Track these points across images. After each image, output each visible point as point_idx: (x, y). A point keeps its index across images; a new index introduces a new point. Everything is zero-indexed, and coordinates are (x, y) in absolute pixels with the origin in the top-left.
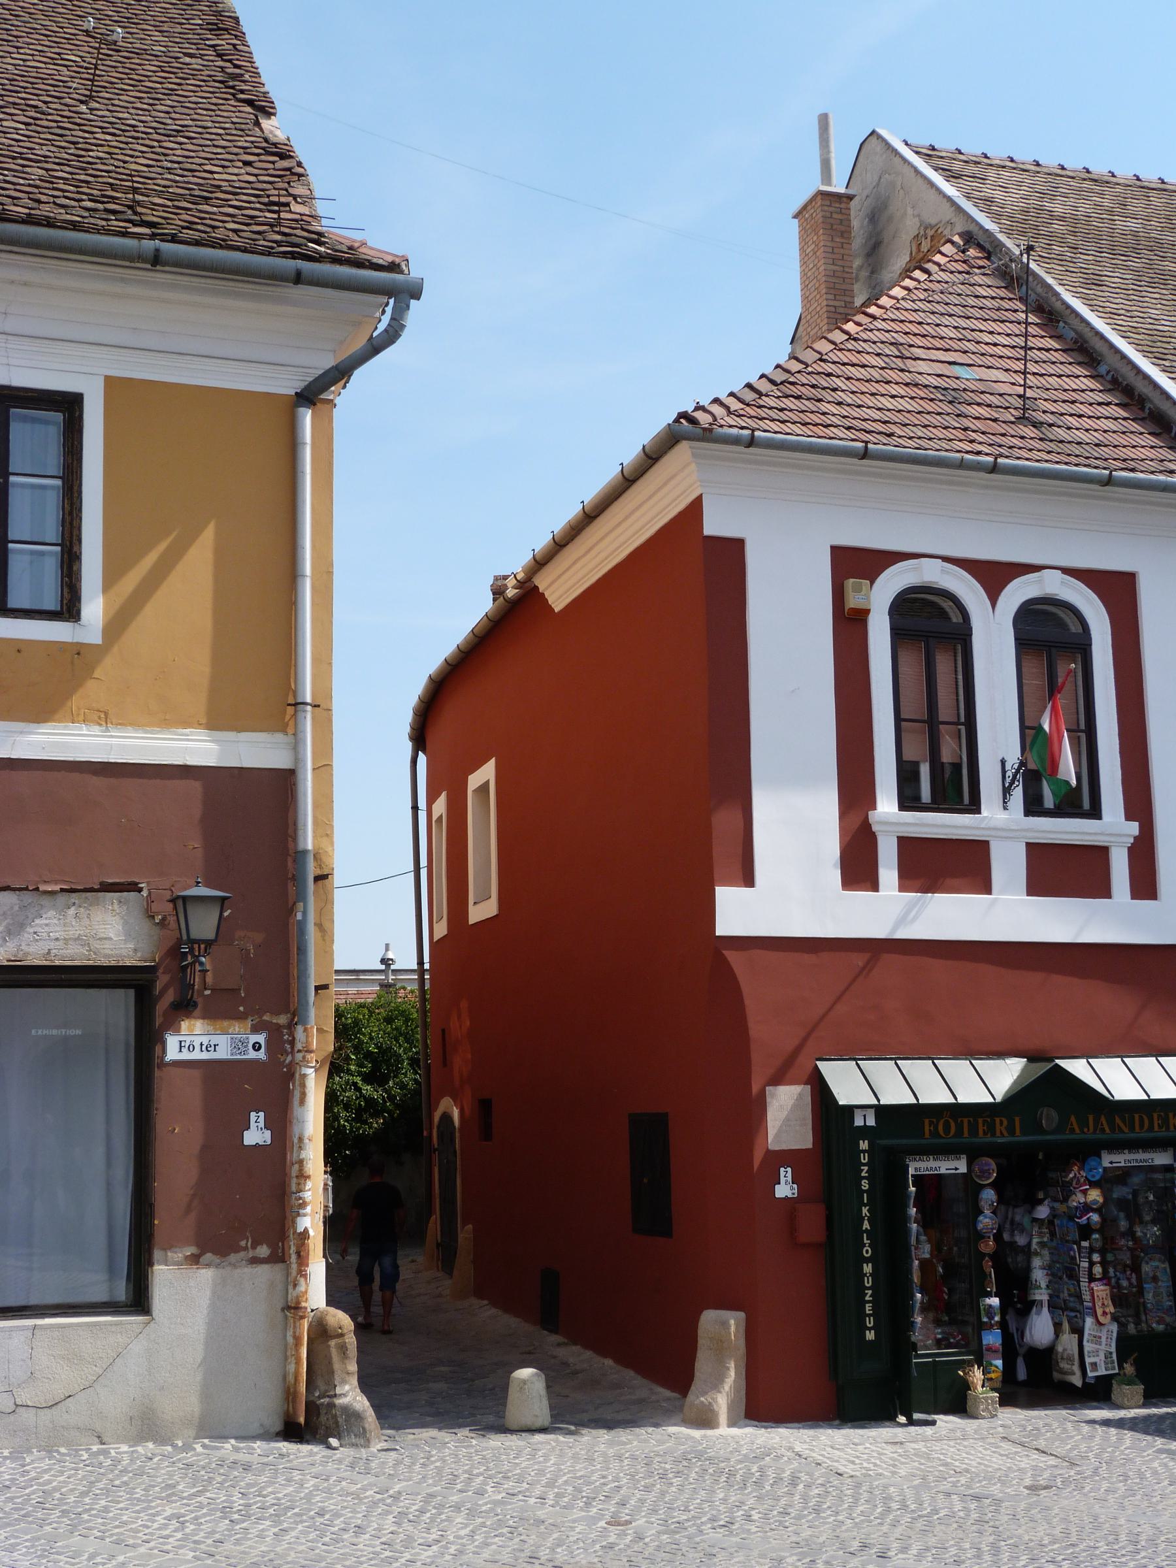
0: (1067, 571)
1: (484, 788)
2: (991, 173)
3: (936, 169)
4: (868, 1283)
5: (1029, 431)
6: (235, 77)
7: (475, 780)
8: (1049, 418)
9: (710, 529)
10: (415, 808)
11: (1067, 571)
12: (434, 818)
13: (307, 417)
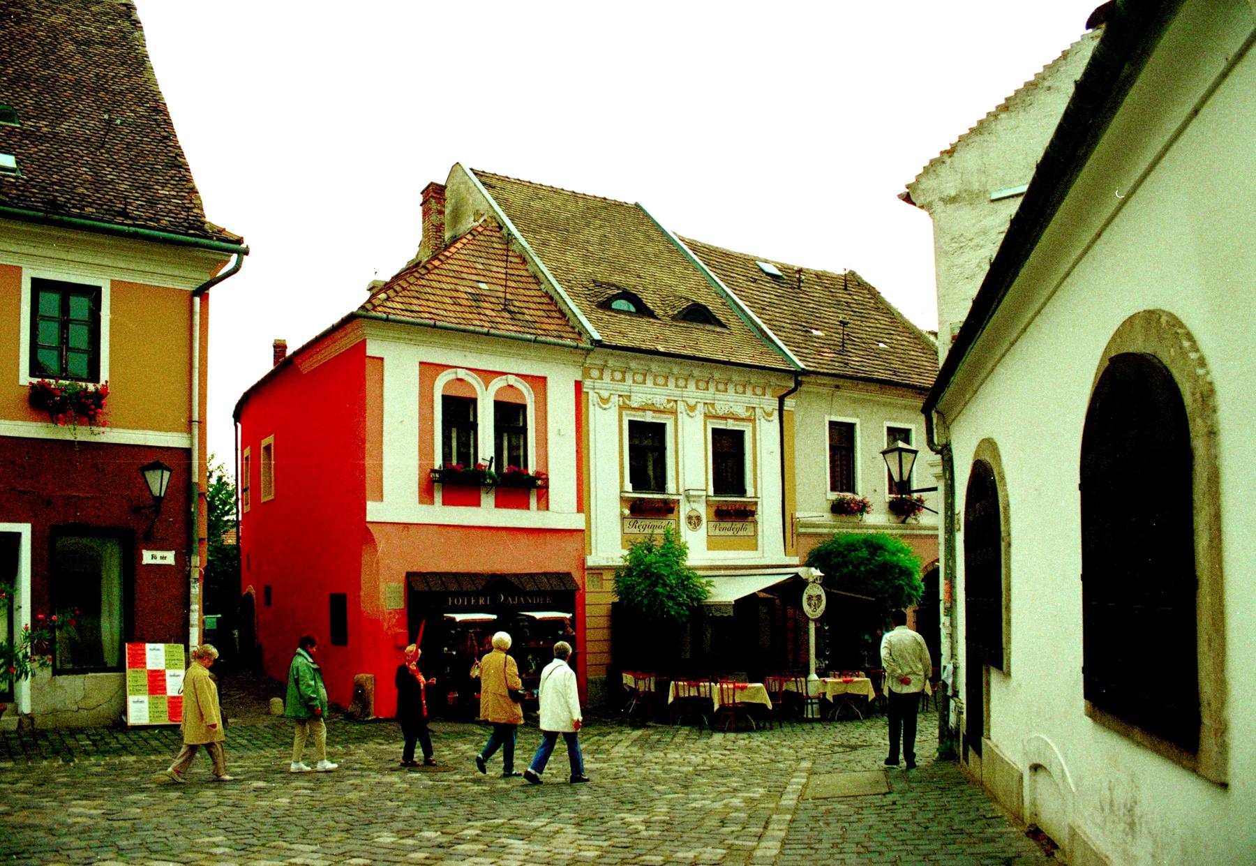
0: (517, 375)
1: (268, 448)
2: (509, 186)
3: (484, 184)
4: (902, 738)
5: (506, 315)
6: (166, 138)
7: (264, 443)
8: (516, 310)
10: (237, 449)
11: (517, 375)
12: (245, 456)
13: (197, 300)
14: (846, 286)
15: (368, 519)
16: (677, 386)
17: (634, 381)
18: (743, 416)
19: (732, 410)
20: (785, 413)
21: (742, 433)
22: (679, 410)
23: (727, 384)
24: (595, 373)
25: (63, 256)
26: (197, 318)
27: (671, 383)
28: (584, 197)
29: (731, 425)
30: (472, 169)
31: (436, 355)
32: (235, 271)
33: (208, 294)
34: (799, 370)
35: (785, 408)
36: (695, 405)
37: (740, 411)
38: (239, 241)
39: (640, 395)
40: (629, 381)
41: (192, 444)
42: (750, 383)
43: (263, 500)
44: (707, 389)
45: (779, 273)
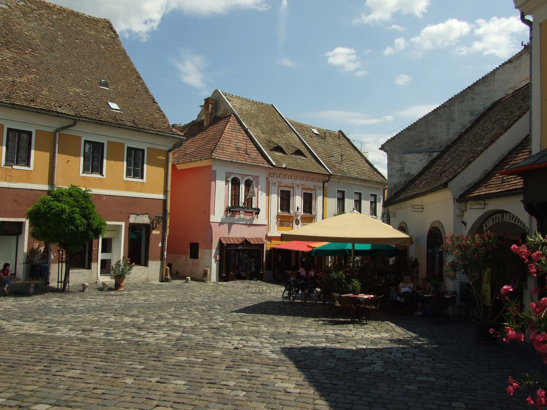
3: (227, 99)
9: (213, 169)
14: (339, 137)
20: (325, 188)
24: (272, 175)
29: (309, 191)
31: (231, 170)
32: (406, 224)
37: (312, 188)
45: (318, 133)
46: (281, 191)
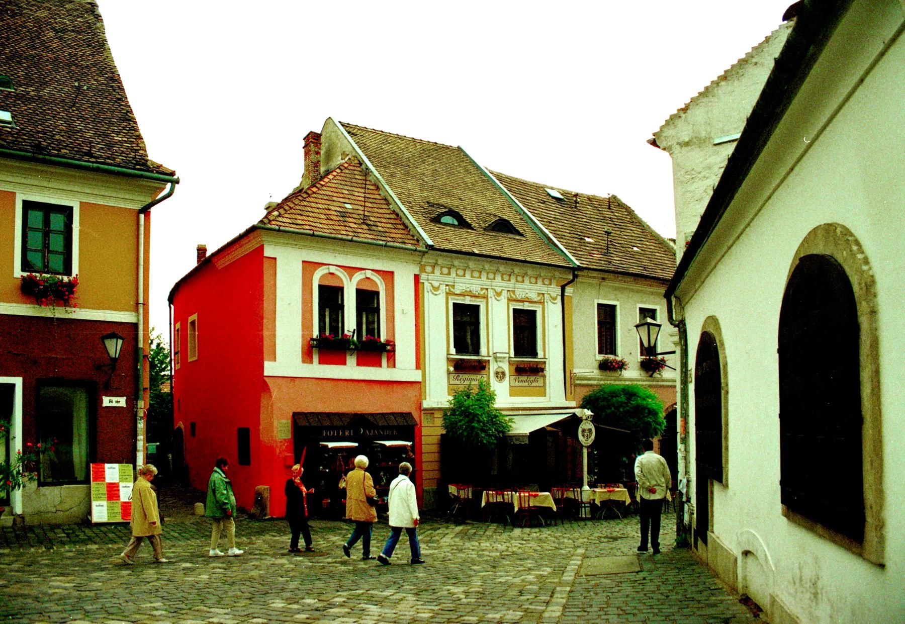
0: (373, 270)
1: (193, 323)
2: (367, 134)
3: (349, 132)
5: (365, 227)
6: (120, 99)
7: (191, 319)
8: (372, 223)
10: (170, 324)
11: (373, 270)
12: (176, 329)
13: (142, 216)
14: (609, 206)
15: (265, 374)
16: (488, 278)
17: (457, 275)
18: (536, 300)
19: (527, 295)
20: (565, 298)
21: (535, 312)
22: (489, 296)
23: (524, 277)
24: (429, 269)
25: (46, 184)
26: (142, 229)
27: (484, 276)
28: (421, 142)
29: (527, 306)
30: (340, 122)
31: (314, 256)
33: (150, 212)
34: (576, 266)
35: (566, 294)
36: (501, 292)
37: (534, 296)
38: (172, 174)
39: (461, 285)
40: (453, 275)
41: (138, 320)
42: (540, 276)
43: (190, 360)
44: (510, 280)
45: (562, 197)
46: (514, 310)
